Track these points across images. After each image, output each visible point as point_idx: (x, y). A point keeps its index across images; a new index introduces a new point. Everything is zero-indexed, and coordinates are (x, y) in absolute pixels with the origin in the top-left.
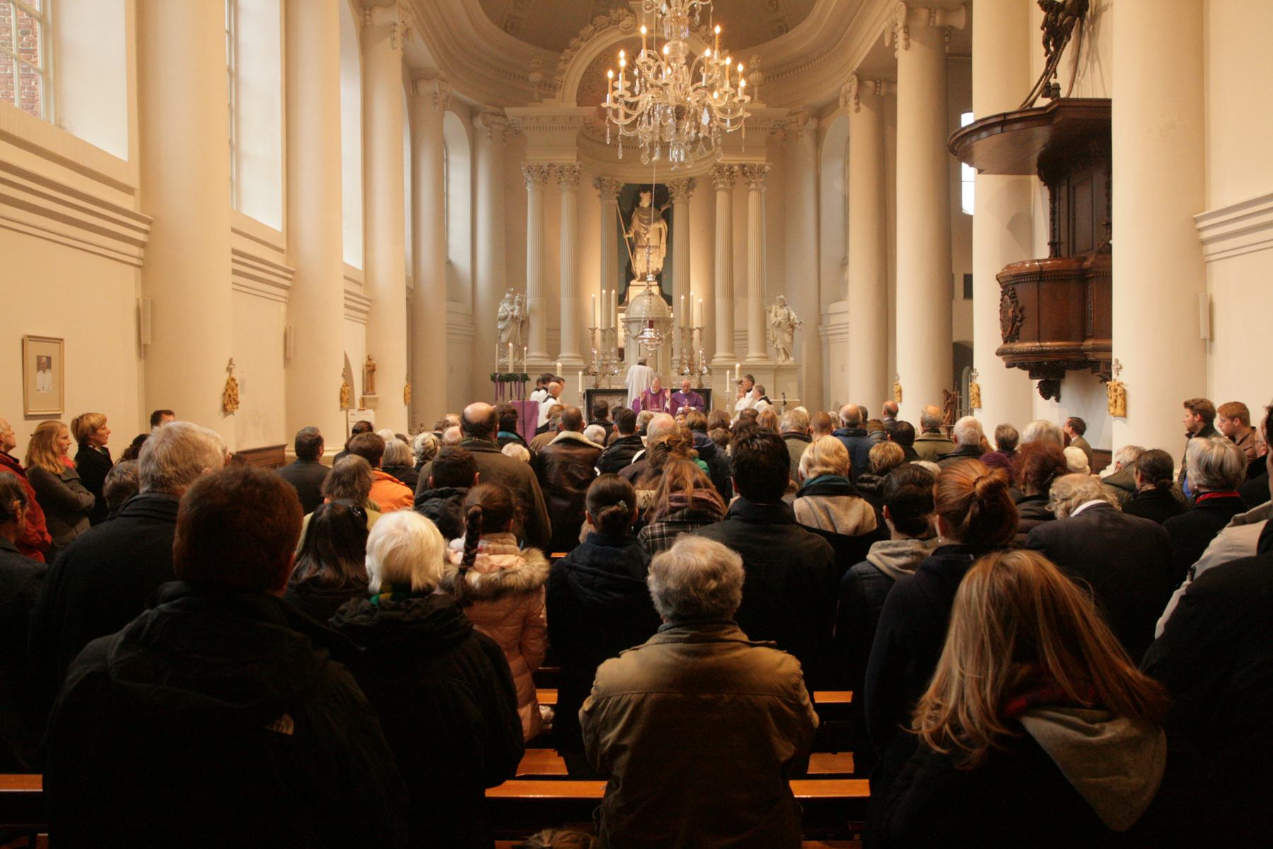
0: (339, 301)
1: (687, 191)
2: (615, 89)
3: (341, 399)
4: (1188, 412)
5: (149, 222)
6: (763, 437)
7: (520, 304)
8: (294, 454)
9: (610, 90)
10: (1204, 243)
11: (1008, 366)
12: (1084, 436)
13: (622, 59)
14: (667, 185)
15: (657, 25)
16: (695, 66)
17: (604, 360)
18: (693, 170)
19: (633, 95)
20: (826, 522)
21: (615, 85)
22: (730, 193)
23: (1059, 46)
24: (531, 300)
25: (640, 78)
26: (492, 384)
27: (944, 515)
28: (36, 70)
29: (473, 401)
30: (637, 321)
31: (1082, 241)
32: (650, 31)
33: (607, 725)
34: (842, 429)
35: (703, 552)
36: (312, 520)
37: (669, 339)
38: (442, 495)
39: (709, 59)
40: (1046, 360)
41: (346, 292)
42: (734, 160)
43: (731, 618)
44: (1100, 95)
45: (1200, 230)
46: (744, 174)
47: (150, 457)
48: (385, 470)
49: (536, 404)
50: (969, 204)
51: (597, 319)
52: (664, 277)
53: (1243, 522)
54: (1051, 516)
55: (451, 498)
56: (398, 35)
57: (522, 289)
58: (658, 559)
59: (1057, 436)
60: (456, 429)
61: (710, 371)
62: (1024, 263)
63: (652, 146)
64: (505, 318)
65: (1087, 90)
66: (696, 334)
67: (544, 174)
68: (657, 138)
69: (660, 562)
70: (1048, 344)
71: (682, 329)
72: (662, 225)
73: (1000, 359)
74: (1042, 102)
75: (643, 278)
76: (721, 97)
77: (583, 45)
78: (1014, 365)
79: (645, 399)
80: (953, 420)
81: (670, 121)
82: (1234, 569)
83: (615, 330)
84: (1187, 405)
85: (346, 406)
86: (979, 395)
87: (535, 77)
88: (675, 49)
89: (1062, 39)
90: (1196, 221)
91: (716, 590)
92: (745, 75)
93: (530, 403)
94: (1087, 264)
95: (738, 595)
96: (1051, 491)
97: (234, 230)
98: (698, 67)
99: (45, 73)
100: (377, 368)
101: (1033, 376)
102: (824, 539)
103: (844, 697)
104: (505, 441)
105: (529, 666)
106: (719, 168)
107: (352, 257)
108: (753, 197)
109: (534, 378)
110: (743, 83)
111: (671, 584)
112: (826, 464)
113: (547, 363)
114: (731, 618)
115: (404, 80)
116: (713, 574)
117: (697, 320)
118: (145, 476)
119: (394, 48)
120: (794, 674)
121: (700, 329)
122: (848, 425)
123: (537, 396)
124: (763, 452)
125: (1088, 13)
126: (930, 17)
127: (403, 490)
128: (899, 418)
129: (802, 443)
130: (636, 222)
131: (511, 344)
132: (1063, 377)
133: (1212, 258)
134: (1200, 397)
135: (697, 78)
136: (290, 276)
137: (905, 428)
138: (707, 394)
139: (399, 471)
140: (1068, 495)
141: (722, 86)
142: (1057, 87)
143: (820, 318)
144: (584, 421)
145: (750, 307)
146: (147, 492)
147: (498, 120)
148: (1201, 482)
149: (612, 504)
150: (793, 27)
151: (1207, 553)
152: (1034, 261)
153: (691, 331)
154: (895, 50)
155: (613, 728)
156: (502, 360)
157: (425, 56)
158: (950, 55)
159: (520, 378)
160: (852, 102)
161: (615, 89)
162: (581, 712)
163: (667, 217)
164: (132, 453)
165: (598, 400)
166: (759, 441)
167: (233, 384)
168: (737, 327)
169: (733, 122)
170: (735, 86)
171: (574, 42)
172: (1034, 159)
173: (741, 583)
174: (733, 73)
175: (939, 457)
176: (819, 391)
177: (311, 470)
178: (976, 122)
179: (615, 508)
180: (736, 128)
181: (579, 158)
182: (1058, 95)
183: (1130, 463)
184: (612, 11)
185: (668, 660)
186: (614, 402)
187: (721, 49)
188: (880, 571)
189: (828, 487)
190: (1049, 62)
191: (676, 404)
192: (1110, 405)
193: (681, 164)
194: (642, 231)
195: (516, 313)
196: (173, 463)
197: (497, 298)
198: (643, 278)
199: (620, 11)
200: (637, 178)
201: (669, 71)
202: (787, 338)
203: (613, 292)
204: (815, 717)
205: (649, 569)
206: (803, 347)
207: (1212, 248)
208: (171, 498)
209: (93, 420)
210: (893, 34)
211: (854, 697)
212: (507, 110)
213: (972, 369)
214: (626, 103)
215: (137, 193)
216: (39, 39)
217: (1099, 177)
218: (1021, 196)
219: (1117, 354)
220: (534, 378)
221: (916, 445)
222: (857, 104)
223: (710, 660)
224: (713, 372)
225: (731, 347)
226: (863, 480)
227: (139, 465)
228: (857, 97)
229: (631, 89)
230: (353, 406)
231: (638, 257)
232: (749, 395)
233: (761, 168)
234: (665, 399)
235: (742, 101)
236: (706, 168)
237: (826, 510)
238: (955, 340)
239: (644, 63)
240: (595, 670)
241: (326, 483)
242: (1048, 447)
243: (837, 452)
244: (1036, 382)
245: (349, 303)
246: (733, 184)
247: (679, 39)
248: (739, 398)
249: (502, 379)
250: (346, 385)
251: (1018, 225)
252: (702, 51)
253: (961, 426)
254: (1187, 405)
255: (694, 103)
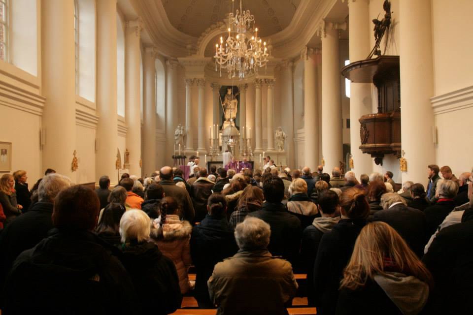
0: (116, 128)
1: (245, 88)
2: (218, 51)
3: (116, 165)
4: (429, 169)
5: (45, 99)
6: (274, 179)
7: (183, 130)
8: (99, 186)
9: (217, 51)
10: (433, 108)
11: (363, 153)
12: (393, 178)
13: (221, 40)
14: (238, 86)
15: (234, 28)
16: (248, 44)
17: (214, 150)
18: (247, 81)
19: (225, 53)
20: (300, 211)
21: (219, 49)
22: (261, 89)
23: (380, 37)
24: (187, 128)
25: (228, 47)
26: (173, 160)
27: (343, 207)
28: (2, 42)
29: (163, 166)
30: (227, 136)
31: (390, 107)
32: (232, 30)
33: (218, 288)
34: (303, 176)
35: (256, 224)
36: (104, 211)
37: (239, 143)
38: (151, 202)
39: (254, 40)
40: (377, 150)
41: (119, 125)
42: (262, 77)
43: (266, 248)
44: (395, 54)
45: (432, 103)
46: (266, 82)
47: (42, 187)
48: (133, 192)
49: (189, 167)
50: (348, 93)
51: (211, 135)
52: (237, 121)
53: (458, 210)
54: (381, 208)
55: (154, 204)
56: (139, 32)
57: (184, 124)
58: (239, 225)
59: (382, 179)
60: (158, 177)
61: (254, 155)
62: (369, 115)
63: (232, 72)
64: (177, 135)
65: (391, 52)
66: (248, 141)
67: (192, 82)
68: (234, 69)
69: (239, 227)
70: (378, 145)
71: (243, 139)
72: (236, 101)
73: (360, 150)
74: (374, 57)
75: (229, 120)
76: (258, 54)
77: (207, 35)
78: (365, 152)
79: (230, 165)
80: (344, 172)
81: (239, 63)
82: (453, 227)
83: (218, 139)
84: (429, 167)
85: (118, 167)
86: (353, 163)
87: (189, 46)
88: (241, 37)
89: (381, 34)
90: (431, 100)
91: (260, 238)
92: (267, 46)
93: (187, 166)
94: (392, 115)
95: (268, 240)
96: (381, 199)
97: (77, 102)
98: (249, 43)
99: (6, 44)
100: (130, 154)
101: (372, 156)
102: (297, 218)
103: (304, 276)
104: (177, 181)
105: (185, 265)
106: (257, 80)
107: (121, 112)
108: (269, 91)
109: (188, 157)
110: (266, 49)
111: (243, 236)
112: (298, 190)
113: (193, 152)
114: (266, 248)
115: (140, 48)
116: (259, 232)
117: (249, 136)
118: (41, 194)
119: (137, 35)
120: (289, 269)
121: (250, 139)
122: (305, 175)
123: (190, 164)
124: (274, 184)
125: (391, 25)
126: (333, 26)
127: (140, 200)
128: (324, 172)
129: (289, 182)
130: (226, 100)
131: (180, 145)
132: (384, 156)
133: (437, 113)
134: (434, 164)
135: (249, 47)
136: (97, 119)
137: (326, 175)
138: (252, 163)
139: (138, 192)
140: (389, 199)
141: (258, 50)
142: (380, 51)
143: (294, 135)
144: (208, 173)
145: (268, 131)
146: (42, 201)
147: (174, 62)
148: (441, 193)
149: (216, 203)
150: (284, 29)
151: (445, 221)
152: (372, 114)
153: (247, 140)
154: (321, 37)
155: (221, 289)
156: (176, 151)
157: (148, 38)
158: (341, 39)
159: (183, 157)
160: (305, 56)
161: (218, 51)
162: (208, 282)
163: (238, 98)
164: (36, 187)
165: (212, 165)
166: (273, 180)
167: (76, 160)
168: (263, 138)
169: (262, 63)
170: (263, 50)
171: (203, 34)
172: (372, 77)
173: (269, 235)
174: (262, 45)
175: (340, 186)
176: (293, 162)
177: (105, 192)
178: (351, 64)
179: (217, 204)
180: (263, 65)
181: (205, 77)
182: (380, 54)
183: (408, 189)
184: (217, 23)
185: (241, 264)
186: (218, 166)
187: (258, 37)
188: (317, 229)
189: (300, 197)
190: (377, 42)
191: (241, 167)
192: (401, 167)
193: (243, 79)
194: (229, 103)
195: (181, 133)
196: (51, 190)
197: (175, 128)
198: (229, 120)
199: (220, 23)
200: (227, 84)
201: (239, 44)
202: (282, 142)
203: (218, 125)
204: (297, 284)
205: (235, 229)
206: (288, 146)
207: (437, 110)
208: (51, 203)
209: (20, 173)
210: (320, 32)
211: (307, 276)
212: (179, 59)
213: (350, 153)
214: (223, 56)
215: (41, 88)
216: (4, 31)
217: (396, 84)
218: (367, 90)
219: (403, 148)
220: (188, 157)
221: (330, 182)
222: (307, 57)
223: (258, 264)
224: (255, 155)
225: (261, 145)
226: (314, 195)
227: (39, 191)
228: (307, 54)
229: (225, 51)
230: (121, 168)
231: (227, 112)
232: (268, 163)
233: (272, 80)
234: (237, 165)
235: (266, 56)
236: (252, 80)
237: (299, 206)
238: (344, 143)
239: (229, 42)
240: (213, 267)
241: (109, 197)
242: (380, 182)
243: (303, 185)
244: (374, 159)
245: (119, 129)
246: (262, 86)
247: (242, 33)
248: (265, 164)
249: (176, 158)
250: (118, 160)
251: (366, 101)
252: (250, 38)
253: (347, 175)
254: (429, 167)
255: (248, 56)
